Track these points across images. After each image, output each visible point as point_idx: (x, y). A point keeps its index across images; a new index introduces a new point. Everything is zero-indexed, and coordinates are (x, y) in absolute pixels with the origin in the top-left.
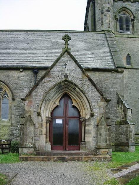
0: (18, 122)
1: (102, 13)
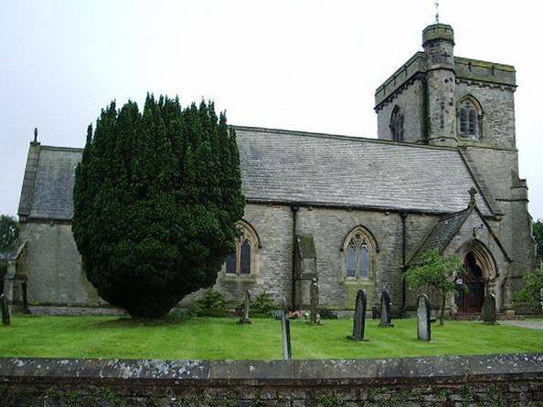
0: (383, 281)
1: (443, 108)
